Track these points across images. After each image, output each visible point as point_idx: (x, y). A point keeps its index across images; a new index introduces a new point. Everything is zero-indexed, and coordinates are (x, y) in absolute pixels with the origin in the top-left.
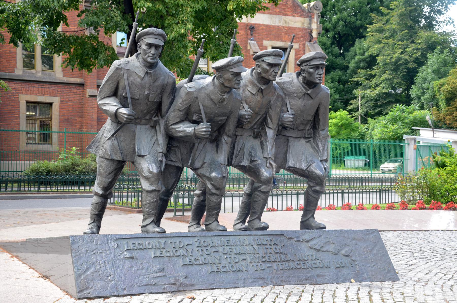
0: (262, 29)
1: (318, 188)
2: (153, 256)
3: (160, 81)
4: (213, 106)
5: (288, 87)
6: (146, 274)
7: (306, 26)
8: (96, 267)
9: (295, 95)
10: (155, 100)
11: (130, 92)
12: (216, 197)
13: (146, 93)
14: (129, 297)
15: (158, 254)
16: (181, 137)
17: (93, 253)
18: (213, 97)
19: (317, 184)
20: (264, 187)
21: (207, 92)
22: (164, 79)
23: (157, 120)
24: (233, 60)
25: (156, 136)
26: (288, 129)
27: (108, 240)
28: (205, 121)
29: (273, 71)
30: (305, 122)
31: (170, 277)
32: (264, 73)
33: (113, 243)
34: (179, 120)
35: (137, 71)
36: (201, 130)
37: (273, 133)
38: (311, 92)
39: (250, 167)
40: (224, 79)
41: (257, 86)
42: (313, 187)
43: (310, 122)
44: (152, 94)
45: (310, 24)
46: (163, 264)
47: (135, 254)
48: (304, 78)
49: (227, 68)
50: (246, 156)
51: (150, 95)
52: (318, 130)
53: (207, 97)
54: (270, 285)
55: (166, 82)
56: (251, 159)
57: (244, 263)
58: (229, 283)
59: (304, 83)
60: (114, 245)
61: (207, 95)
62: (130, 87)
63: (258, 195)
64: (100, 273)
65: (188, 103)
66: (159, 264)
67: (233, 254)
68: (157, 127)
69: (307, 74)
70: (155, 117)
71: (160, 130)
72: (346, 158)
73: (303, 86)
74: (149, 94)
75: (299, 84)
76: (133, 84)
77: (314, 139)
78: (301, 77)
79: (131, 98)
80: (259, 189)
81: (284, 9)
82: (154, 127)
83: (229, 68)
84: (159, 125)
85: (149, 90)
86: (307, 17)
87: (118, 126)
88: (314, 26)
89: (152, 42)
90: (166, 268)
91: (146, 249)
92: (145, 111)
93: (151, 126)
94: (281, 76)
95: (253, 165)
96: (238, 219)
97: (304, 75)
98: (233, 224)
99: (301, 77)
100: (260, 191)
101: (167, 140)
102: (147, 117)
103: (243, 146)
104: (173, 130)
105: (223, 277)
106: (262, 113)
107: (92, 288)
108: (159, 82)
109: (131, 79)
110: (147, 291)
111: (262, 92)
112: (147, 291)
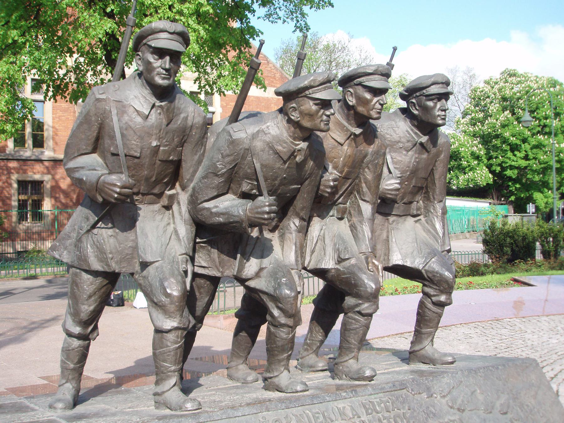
0: (252, 100)
1: (443, 298)
3: (179, 122)
4: (279, 165)
5: (389, 132)
9: (401, 145)
10: (171, 158)
11: (124, 144)
12: (285, 330)
13: (154, 144)
16: (221, 225)
18: (279, 148)
19: (442, 292)
20: (366, 305)
21: (268, 139)
22: (186, 118)
23: (174, 194)
25: (174, 223)
28: (265, 192)
29: (378, 101)
34: (216, 194)
36: (259, 210)
37: (372, 209)
39: (337, 270)
40: (301, 113)
41: (348, 130)
42: (434, 296)
44: (166, 146)
49: (307, 92)
50: (330, 250)
51: (161, 148)
52: (434, 202)
53: (267, 149)
55: (190, 123)
56: (339, 257)
61: (268, 144)
62: (123, 135)
63: (355, 319)
65: (234, 160)
68: (175, 207)
70: (169, 190)
71: (180, 213)
73: (412, 130)
74: (159, 146)
76: (128, 127)
77: (425, 216)
79: (126, 156)
80: (357, 309)
81: (272, 82)
82: (168, 208)
83: (310, 91)
84: (179, 203)
85: (159, 139)
87: (346, 134)
92: (154, 179)
93: (164, 207)
95: (344, 268)
100: (359, 313)
101: (194, 229)
102: (156, 191)
103: (322, 234)
104: (205, 213)
108: (178, 122)
109: (126, 118)
111: (354, 139)
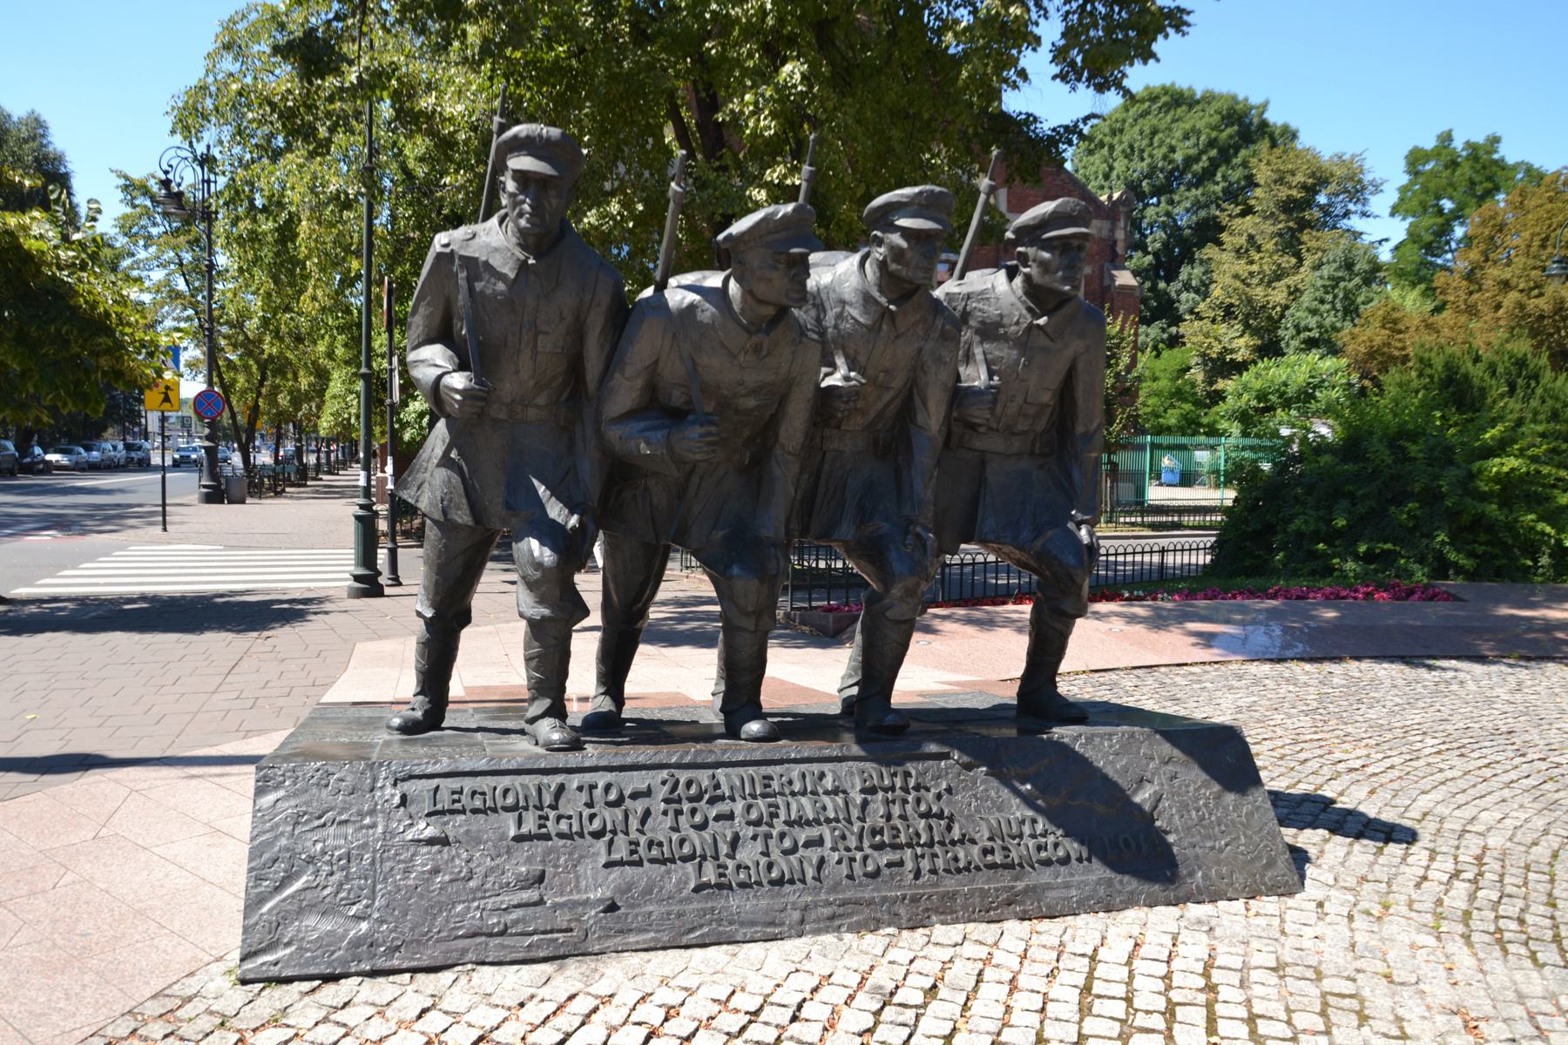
2: (512, 833)
6: (479, 895)
7: (1105, 233)
8: (317, 873)
14: (407, 976)
15: (530, 825)
17: (317, 823)
24: (775, 213)
26: (982, 429)
27: (375, 780)
30: (1032, 411)
31: (555, 907)
32: (894, 261)
33: (389, 791)
35: (496, 262)
38: (1047, 324)
43: (1049, 410)
45: (1112, 230)
46: (543, 861)
47: (456, 826)
48: (1028, 279)
54: (889, 925)
57: (813, 854)
58: (753, 923)
59: (1026, 293)
60: (393, 796)
64: (326, 892)
66: (529, 860)
67: (779, 825)
69: (1034, 265)
72: (836, 709)
75: (1013, 299)
78: (1018, 281)
86: (1107, 218)
88: (1120, 235)
89: (525, 168)
90: (550, 870)
91: (495, 810)
94: (962, 277)
96: (850, 676)
97: (1027, 270)
98: (838, 686)
99: (1018, 281)
105: (735, 902)
106: (897, 383)
107: (288, 944)
110: (471, 956)
112: (471, 956)
